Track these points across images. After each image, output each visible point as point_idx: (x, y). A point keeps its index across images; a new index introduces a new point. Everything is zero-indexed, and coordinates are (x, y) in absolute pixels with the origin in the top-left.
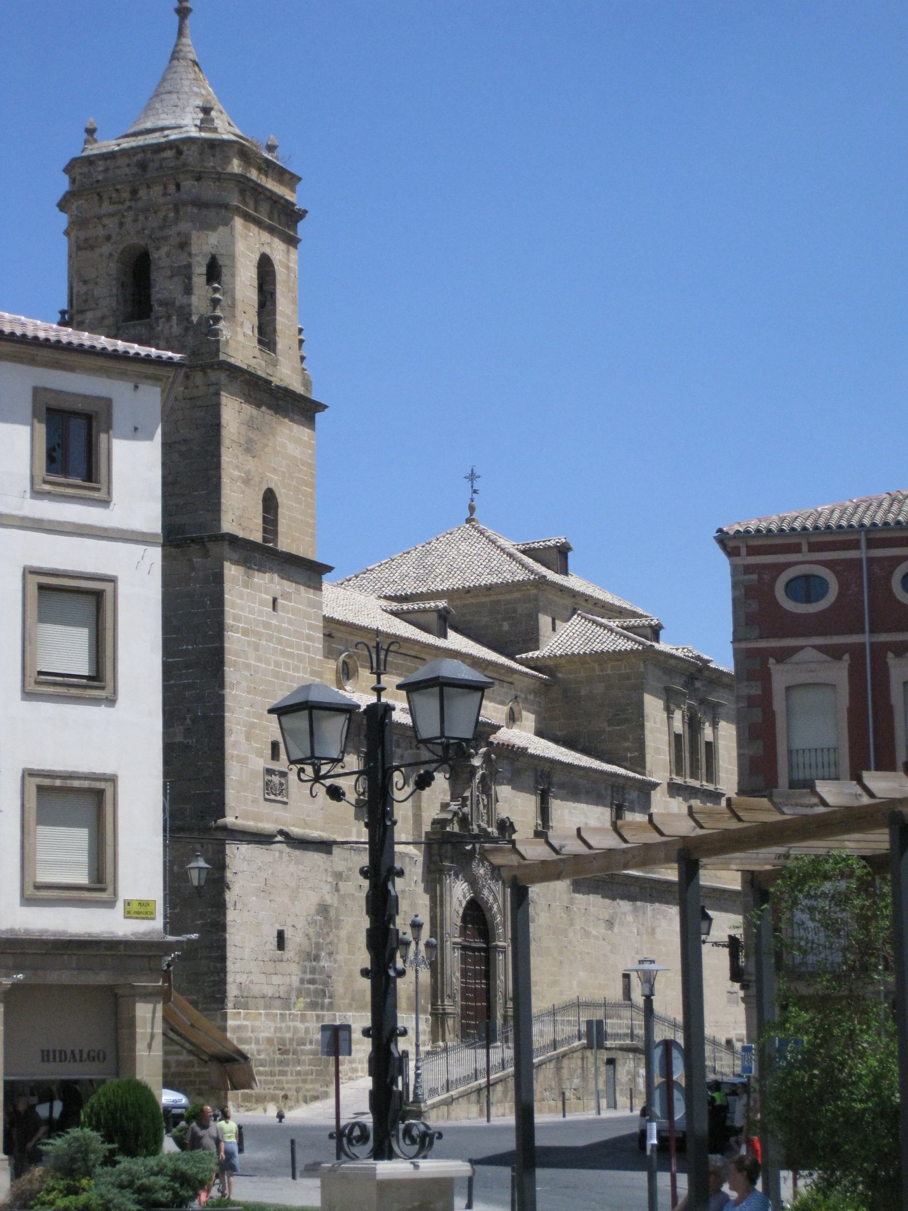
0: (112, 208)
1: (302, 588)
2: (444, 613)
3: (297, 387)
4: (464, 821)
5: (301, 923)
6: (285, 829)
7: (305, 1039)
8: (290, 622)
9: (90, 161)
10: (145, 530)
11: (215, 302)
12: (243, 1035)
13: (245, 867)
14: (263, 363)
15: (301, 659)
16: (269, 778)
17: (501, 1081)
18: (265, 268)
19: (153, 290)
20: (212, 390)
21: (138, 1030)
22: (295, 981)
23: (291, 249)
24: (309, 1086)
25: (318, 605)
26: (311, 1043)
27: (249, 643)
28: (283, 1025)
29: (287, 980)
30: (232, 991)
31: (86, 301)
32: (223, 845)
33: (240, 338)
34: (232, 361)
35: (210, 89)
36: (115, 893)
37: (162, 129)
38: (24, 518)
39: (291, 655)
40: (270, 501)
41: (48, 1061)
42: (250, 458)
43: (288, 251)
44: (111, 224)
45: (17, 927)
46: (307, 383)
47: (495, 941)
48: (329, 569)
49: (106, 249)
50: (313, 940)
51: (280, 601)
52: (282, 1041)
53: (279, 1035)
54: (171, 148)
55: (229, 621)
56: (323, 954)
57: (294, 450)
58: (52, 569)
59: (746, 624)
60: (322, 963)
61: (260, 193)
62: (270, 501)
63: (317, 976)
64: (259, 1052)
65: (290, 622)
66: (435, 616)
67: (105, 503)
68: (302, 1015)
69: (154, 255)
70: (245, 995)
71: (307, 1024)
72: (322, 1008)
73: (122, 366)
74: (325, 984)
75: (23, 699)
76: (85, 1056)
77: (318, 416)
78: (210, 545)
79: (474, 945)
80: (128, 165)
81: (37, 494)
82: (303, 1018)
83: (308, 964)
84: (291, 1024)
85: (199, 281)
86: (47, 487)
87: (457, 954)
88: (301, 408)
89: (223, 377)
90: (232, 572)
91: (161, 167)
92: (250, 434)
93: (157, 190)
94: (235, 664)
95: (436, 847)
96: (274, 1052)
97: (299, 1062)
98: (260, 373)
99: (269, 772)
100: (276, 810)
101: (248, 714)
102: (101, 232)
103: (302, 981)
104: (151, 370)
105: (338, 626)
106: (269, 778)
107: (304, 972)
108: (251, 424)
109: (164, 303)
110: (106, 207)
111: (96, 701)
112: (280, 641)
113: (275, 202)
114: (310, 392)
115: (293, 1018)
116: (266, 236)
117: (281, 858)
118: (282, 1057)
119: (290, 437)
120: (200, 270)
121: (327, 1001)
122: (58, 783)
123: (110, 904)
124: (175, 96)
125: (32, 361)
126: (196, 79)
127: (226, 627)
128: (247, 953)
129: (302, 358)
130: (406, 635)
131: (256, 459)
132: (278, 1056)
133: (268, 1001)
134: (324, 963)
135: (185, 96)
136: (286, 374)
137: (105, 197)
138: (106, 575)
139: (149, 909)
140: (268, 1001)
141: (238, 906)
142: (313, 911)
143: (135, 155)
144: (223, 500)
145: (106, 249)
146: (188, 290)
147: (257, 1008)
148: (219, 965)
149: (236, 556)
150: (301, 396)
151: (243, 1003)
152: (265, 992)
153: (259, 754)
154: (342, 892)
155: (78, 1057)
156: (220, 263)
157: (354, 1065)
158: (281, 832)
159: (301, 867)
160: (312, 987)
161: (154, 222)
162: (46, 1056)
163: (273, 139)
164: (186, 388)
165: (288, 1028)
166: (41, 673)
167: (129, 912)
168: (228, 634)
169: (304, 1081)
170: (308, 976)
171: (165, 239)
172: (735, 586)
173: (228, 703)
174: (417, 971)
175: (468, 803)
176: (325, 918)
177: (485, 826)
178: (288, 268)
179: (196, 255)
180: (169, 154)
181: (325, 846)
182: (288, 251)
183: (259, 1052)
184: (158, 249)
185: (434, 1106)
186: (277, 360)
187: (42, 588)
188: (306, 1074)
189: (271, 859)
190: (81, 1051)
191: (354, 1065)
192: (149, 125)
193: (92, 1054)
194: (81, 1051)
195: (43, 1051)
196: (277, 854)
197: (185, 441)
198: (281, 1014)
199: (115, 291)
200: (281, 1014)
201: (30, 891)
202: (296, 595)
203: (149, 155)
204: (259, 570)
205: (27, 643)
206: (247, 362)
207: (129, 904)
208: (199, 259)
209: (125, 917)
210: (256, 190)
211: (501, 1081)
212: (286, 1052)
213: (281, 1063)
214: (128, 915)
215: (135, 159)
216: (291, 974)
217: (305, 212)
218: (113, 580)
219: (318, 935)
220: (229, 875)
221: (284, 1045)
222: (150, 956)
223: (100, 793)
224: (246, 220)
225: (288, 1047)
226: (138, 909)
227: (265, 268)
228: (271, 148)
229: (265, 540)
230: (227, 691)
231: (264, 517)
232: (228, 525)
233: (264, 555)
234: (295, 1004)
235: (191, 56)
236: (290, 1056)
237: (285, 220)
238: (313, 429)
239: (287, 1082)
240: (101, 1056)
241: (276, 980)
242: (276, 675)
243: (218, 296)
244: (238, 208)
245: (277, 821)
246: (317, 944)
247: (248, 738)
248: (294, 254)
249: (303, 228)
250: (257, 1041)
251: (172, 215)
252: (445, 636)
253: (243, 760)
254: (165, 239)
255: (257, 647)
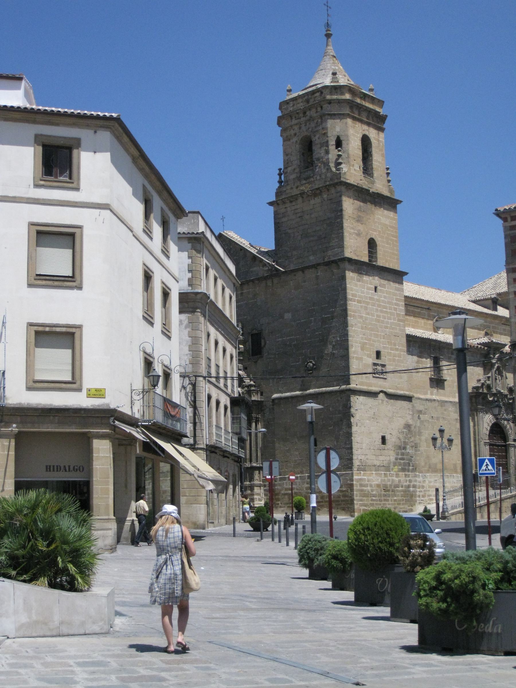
0: (296, 121)
1: (392, 283)
2: (495, 300)
3: (386, 192)
4: (489, 387)
5: (395, 433)
6: (385, 390)
7: (399, 485)
8: (385, 297)
9: (287, 102)
10: (100, 202)
11: (339, 156)
12: (363, 483)
13: (362, 407)
14: (366, 183)
15: (391, 314)
16: (376, 367)
17: (494, 502)
18: (366, 142)
19: (314, 154)
20: (338, 194)
21: (94, 455)
22: (393, 459)
23: (380, 133)
24: (402, 506)
25: (402, 290)
26: (402, 487)
27: (361, 306)
28: (386, 479)
29: (388, 458)
30: (356, 463)
31: (288, 163)
32: (350, 397)
33: (352, 171)
34: (348, 181)
35: (341, 67)
36: (81, 385)
37: (316, 85)
38: (28, 198)
39: (386, 312)
40: (372, 244)
41: (50, 471)
42: (360, 225)
43: (378, 133)
44: (296, 128)
45: (23, 402)
46: (391, 191)
47: (508, 441)
48: (406, 274)
49: (295, 139)
50: (402, 440)
51: (379, 288)
52: (385, 486)
53: (383, 483)
54: (318, 92)
55: (349, 296)
56: (408, 447)
57: (383, 220)
58: (44, 223)
59: (512, 256)
60: (408, 451)
61: (361, 108)
62: (372, 244)
63: (405, 457)
64: (372, 491)
65: (385, 297)
66: (490, 301)
67: (77, 189)
68: (396, 474)
69: (313, 139)
70: (364, 465)
71: (399, 478)
72: (408, 471)
73: (89, 122)
74: (410, 460)
75: (28, 287)
76: (72, 468)
77: (398, 206)
78: (339, 263)
79: (498, 444)
80: (302, 102)
81: (36, 186)
82: (397, 475)
83: (400, 451)
84: (390, 478)
85: (332, 147)
86: (42, 183)
87: (488, 447)
88: (390, 203)
89: (343, 188)
90: (350, 275)
91: (315, 101)
92: (359, 214)
93: (314, 110)
94: (354, 316)
95: (474, 399)
96: (381, 491)
97: (395, 496)
98: (364, 187)
99: (375, 364)
100: (380, 382)
101: (362, 338)
102: (292, 132)
103: (396, 459)
104: (101, 123)
105: (432, 304)
106: (376, 367)
107: (397, 454)
108: (359, 209)
109: (318, 159)
110: (294, 121)
111: (71, 288)
112: (379, 306)
113: (370, 111)
114: (394, 195)
115: (392, 475)
116: (365, 127)
117: (382, 403)
118: (385, 493)
119: (382, 217)
120: (332, 142)
121: (411, 468)
122: (47, 329)
123: (80, 390)
124: (324, 71)
125: (35, 122)
126: (333, 63)
127: (348, 299)
128: (364, 446)
129: (389, 181)
130: (468, 308)
131: (363, 225)
132: (383, 493)
133: (377, 468)
134: (409, 450)
135: (328, 70)
136: (379, 186)
137: (293, 117)
138: (75, 225)
139: (102, 393)
140: (377, 468)
141: (359, 424)
142: (402, 427)
143: (304, 97)
144: (345, 243)
145: (295, 139)
146: (327, 152)
147: (371, 471)
148: (349, 451)
149: (353, 268)
150: (387, 197)
151: (363, 468)
152: (375, 463)
153: (369, 356)
154: (422, 419)
155: (67, 470)
156: (342, 139)
157: (431, 497)
158: (382, 391)
159: (394, 407)
160: (402, 461)
161: (313, 125)
162: (48, 468)
163: (371, 86)
164: (328, 195)
165: (389, 480)
166: (37, 275)
167: (89, 395)
168: (349, 302)
169: (399, 504)
170: (400, 457)
171: (317, 131)
172: (506, 237)
173: (350, 333)
174: (442, 452)
175: (491, 379)
176: (409, 431)
177: (500, 389)
178: (378, 141)
179: (331, 137)
180: (318, 94)
181: (408, 399)
182: (378, 133)
183: (372, 491)
184: (315, 136)
185: (453, 514)
186: (374, 181)
187: (39, 233)
188: (400, 500)
189: (377, 404)
190: (69, 466)
191: (431, 497)
192: (312, 84)
193: (76, 468)
194: (69, 466)
195: (47, 466)
196: (380, 401)
197: (329, 219)
198: (384, 474)
199: (299, 157)
200: (384, 474)
201: (31, 384)
202: (388, 287)
203: (310, 96)
204: (366, 275)
205: (30, 260)
206: (357, 182)
207: (89, 390)
208: (332, 138)
209: (87, 397)
210: (358, 106)
211: (494, 502)
212: (388, 491)
213: (385, 495)
214: (89, 396)
215: (304, 99)
216: (390, 455)
217: (387, 116)
218: (80, 227)
219: (405, 438)
220: (353, 410)
221: (387, 488)
222: (102, 417)
223: (73, 334)
224: (353, 120)
225: (389, 489)
226: (95, 393)
227: (366, 142)
228: (371, 90)
229: (370, 260)
230: (349, 328)
231: (369, 251)
232: (348, 253)
233: (369, 267)
234: (392, 469)
235: (332, 54)
236: (390, 493)
237: (378, 121)
238: (396, 212)
239: (389, 504)
240: (81, 469)
241: (381, 458)
242: (378, 321)
243: (340, 153)
244: (348, 115)
245: (380, 387)
246: (404, 442)
247: (362, 349)
248: (382, 135)
249: (386, 125)
250: (371, 486)
251: (319, 120)
252: (496, 310)
253: (360, 359)
254: (317, 131)
255: (366, 309)
